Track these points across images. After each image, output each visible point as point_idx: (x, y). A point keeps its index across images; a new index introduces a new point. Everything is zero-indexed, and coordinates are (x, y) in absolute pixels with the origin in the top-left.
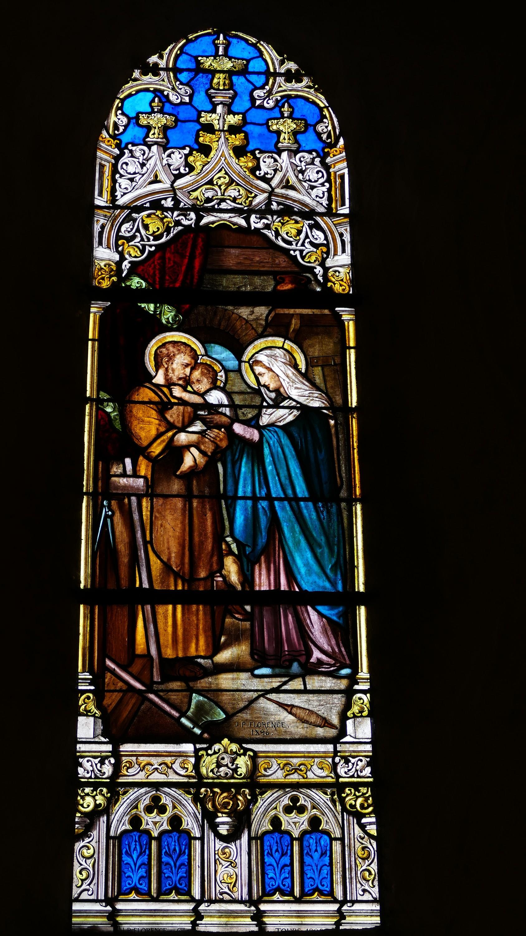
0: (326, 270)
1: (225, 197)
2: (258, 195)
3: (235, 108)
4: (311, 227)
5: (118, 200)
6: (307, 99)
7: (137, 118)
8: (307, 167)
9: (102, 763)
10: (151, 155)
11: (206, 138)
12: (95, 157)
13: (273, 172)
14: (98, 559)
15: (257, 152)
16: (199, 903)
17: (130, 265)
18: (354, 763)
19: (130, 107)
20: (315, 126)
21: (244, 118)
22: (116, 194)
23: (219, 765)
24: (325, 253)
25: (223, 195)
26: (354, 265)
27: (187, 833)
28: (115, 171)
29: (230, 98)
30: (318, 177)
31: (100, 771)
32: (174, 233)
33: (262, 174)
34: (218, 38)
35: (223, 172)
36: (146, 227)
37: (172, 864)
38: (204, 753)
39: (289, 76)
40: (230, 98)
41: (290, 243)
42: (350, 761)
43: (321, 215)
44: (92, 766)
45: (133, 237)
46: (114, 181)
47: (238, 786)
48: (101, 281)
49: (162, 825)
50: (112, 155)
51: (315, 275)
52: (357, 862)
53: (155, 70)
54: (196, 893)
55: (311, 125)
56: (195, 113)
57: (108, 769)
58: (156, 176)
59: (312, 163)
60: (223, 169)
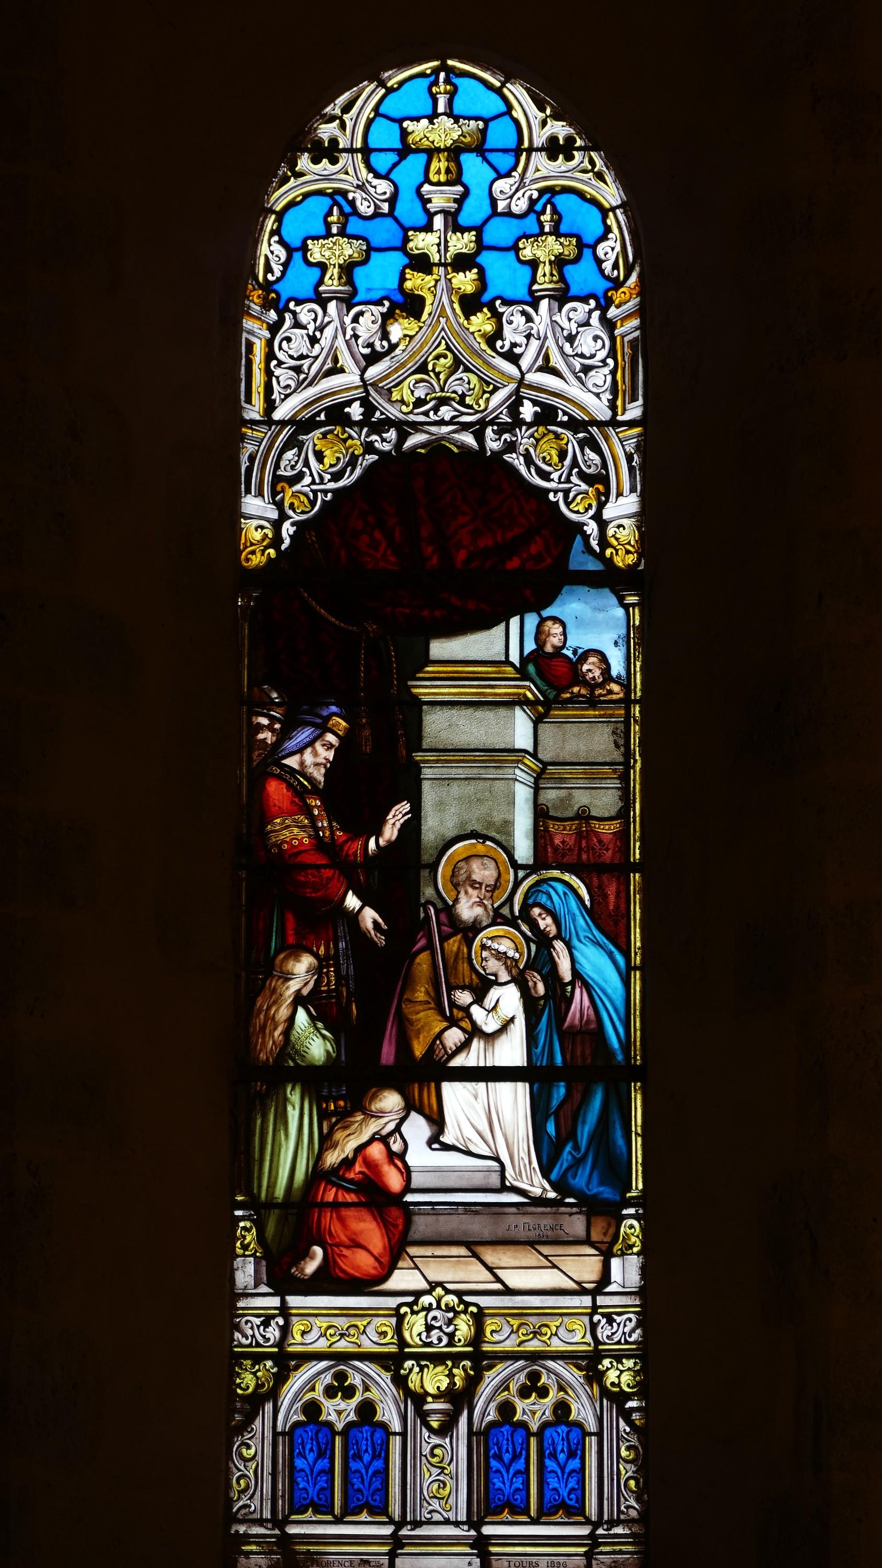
0: (603, 524)
1: (448, 394)
2: (499, 388)
3: (463, 219)
4: (582, 444)
5: (277, 407)
6: (580, 194)
7: (304, 249)
8: (580, 329)
9: (266, 1324)
10: (327, 319)
11: (416, 281)
12: (239, 329)
13: (525, 341)
14: (275, 916)
15: (498, 302)
16: (399, 1525)
17: (295, 528)
18: (620, 1323)
19: (293, 229)
20: (594, 247)
21: (479, 240)
22: (273, 397)
23: (429, 1328)
24: (603, 494)
25: (442, 390)
26: (643, 517)
27: (384, 1426)
28: (270, 355)
29: (455, 201)
30: (597, 349)
31: (264, 1337)
32: (364, 464)
33: (507, 348)
34: (435, 83)
35: (443, 346)
36: (320, 457)
37: (363, 1471)
38: (408, 1310)
39: (553, 149)
40: (455, 201)
41: (545, 476)
42: (615, 1321)
43: (600, 424)
44: (252, 1328)
45: (300, 477)
46: (269, 373)
47: (457, 1358)
48: (250, 556)
49: (348, 1415)
50: (268, 323)
51: (586, 538)
52: (621, 1466)
53: (330, 152)
54: (395, 1510)
55: (588, 246)
56: (399, 234)
57: (273, 1333)
58: (336, 360)
59: (587, 324)
60: (443, 342)
